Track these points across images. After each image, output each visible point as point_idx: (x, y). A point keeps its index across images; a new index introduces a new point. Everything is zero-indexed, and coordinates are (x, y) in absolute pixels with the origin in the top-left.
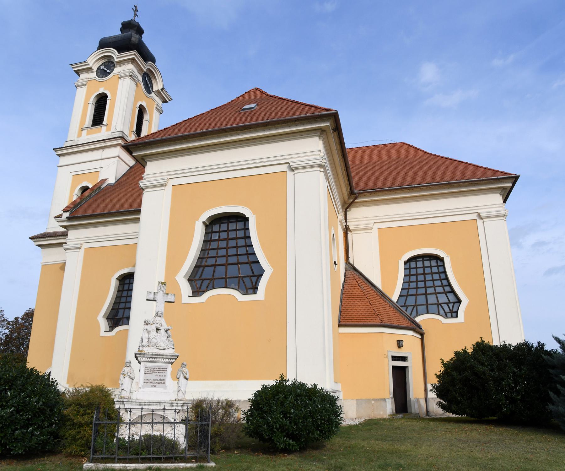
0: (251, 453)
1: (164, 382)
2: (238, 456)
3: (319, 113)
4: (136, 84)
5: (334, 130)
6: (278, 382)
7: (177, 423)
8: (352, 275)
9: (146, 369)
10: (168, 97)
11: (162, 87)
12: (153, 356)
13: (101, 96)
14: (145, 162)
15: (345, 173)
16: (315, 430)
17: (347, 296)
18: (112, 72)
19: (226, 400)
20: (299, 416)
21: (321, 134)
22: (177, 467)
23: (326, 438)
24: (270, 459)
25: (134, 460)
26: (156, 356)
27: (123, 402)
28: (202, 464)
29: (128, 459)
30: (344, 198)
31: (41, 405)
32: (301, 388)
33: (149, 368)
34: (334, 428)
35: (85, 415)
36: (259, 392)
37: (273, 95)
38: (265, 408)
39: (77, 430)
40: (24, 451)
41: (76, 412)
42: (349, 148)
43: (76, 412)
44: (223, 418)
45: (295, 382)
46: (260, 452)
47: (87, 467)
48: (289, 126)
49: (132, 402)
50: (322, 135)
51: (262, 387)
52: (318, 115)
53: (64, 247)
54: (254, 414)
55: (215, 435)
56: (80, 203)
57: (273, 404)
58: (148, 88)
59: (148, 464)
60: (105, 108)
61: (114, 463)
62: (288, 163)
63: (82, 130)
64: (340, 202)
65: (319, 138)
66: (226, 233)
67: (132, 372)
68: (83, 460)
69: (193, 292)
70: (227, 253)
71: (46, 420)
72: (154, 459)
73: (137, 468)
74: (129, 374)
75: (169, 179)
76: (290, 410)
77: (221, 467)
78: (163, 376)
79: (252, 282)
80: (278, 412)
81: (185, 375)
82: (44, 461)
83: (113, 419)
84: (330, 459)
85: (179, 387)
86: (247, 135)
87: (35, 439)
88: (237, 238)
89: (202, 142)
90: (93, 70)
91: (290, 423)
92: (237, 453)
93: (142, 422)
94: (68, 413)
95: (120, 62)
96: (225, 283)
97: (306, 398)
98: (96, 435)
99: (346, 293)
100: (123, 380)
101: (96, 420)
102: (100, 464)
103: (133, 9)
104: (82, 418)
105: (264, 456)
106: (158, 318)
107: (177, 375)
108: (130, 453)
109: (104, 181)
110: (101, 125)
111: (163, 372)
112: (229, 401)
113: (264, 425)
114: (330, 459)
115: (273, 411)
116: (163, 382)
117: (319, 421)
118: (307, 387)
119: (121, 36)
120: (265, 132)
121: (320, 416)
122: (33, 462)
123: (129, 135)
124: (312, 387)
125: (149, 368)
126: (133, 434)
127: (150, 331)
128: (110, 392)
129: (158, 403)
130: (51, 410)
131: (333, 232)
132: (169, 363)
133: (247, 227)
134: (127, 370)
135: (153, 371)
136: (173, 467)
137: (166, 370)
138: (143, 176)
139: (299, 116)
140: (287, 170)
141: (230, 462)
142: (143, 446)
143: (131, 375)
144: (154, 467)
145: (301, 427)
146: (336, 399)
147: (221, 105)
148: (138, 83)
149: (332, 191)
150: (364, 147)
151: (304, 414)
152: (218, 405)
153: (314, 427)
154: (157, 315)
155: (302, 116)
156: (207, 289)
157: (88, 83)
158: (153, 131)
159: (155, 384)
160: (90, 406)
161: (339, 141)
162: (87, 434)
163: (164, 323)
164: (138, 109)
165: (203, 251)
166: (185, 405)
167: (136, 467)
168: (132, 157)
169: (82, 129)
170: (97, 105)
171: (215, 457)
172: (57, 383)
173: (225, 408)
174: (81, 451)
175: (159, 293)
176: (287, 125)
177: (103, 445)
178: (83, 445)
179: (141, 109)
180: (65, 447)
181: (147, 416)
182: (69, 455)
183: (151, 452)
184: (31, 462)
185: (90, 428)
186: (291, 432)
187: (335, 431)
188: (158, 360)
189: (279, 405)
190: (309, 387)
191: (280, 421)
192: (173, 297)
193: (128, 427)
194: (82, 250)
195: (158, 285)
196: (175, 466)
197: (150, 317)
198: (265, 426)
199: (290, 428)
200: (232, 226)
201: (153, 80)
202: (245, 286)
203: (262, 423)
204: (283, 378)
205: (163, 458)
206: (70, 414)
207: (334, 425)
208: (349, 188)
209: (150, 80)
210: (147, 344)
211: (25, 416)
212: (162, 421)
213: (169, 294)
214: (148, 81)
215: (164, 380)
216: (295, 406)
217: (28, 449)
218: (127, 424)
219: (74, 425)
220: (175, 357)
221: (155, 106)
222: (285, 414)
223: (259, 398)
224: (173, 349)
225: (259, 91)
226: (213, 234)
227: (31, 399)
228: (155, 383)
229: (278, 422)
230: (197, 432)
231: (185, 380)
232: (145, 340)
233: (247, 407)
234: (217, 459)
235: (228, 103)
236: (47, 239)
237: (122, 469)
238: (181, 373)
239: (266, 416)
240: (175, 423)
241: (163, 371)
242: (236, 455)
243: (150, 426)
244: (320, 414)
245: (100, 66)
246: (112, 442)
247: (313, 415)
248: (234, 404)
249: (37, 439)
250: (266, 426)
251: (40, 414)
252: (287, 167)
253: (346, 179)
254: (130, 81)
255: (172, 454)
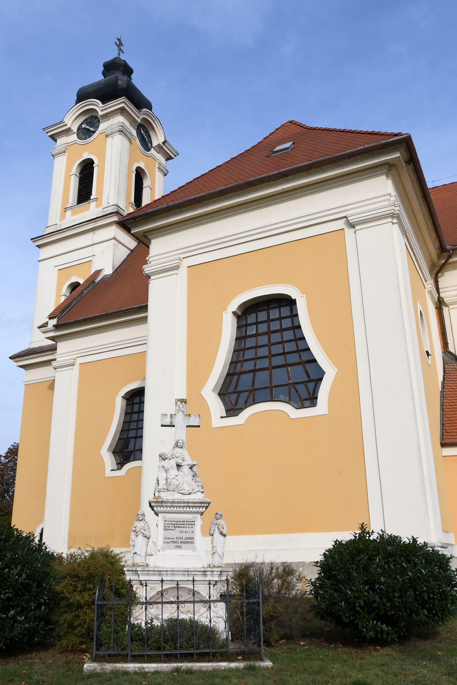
0: (325, 644)
1: (192, 540)
2: (306, 649)
3: (383, 141)
4: (130, 140)
5: (408, 162)
6: (357, 535)
7: (214, 601)
8: (454, 369)
9: (166, 523)
10: (173, 151)
11: (163, 140)
12: (175, 505)
13: (86, 163)
14: (148, 240)
15: (429, 222)
16: (420, 609)
17: (450, 401)
18: (97, 130)
19: (283, 564)
20: (394, 588)
21: (389, 170)
22: (216, 668)
23: (439, 622)
24: (354, 654)
25: (155, 657)
26: (179, 505)
27: (136, 571)
28: (252, 663)
29: (146, 656)
30: (431, 259)
31: (25, 579)
32: (392, 543)
33: (170, 521)
34: (449, 606)
35: (85, 591)
36: (329, 551)
37: (315, 126)
38: (341, 575)
39: (75, 613)
40: (4, 644)
41: (71, 588)
42: (432, 187)
43: (71, 588)
44: (279, 592)
45: (383, 535)
46: (338, 643)
47: (89, 668)
48: (342, 166)
49: (148, 571)
50: (391, 172)
51: (333, 543)
52: (382, 144)
53: (53, 364)
54: (324, 585)
55: (270, 618)
56: (69, 305)
57: (353, 570)
58: (146, 143)
59: (175, 663)
60: (93, 178)
61: (126, 662)
62: (346, 217)
63: (65, 211)
64: (427, 265)
65: (387, 177)
66: (266, 325)
67: (146, 528)
68: (85, 657)
69: (227, 411)
70: (270, 352)
71: (33, 600)
72: (183, 655)
73: (159, 669)
74: (143, 531)
75: (182, 259)
76: (379, 579)
77: (281, 669)
78: (191, 532)
79: (308, 390)
80: (361, 582)
81: (221, 529)
82: (31, 659)
83: (123, 597)
84: (449, 656)
85: (213, 548)
86: (284, 185)
87: (18, 628)
88: (281, 330)
89: (222, 203)
90: (73, 131)
91: (381, 598)
92: (304, 645)
93: (163, 601)
94: (62, 589)
95: (106, 115)
96: (270, 394)
97: (403, 559)
98: (100, 620)
99: (449, 396)
100: (135, 540)
101: (98, 600)
102: (107, 665)
103: (116, 43)
104: (81, 596)
105: (346, 649)
106: (178, 450)
107: (210, 530)
108: (149, 646)
109: (98, 272)
110: (89, 201)
111: (190, 526)
112: (288, 566)
113: (342, 602)
114: (449, 656)
115: (353, 580)
116: (190, 541)
117: (425, 594)
118: (402, 543)
119: (104, 81)
120: (307, 179)
121: (425, 586)
122: (16, 661)
123: (126, 209)
124: (410, 542)
125: (170, 521)
126: (152, 618)
127: (168, 469)
128: (118, 557)
129: (185, 571)
130: (39, 586)
131: (420, 308)
132: (197, 513)
133: (294, 313)
134: (139, 525)
135: (176, 526)
136: (211, 668)
137: (193, 523)
138: (147, 258)
139: (354, 150)
140: (344, 227)
141: (294, 660)
142: (167, 637)
143: (146, 533)
144: (184, 668)
145: (397, 604)
146: (449, 559)
147: (244, 151)
148: (132, 140)
149: (412, 250)
150: (454, 183)
151: (402, 584)
152: (271, 573)
153: (418, 605)
154: (177, 446)
155: (358, 148)
156: (247, 405)
157: (67, 149)
158: (157, 197)
159: (180, 544)
160: (90, 578)
161: (417, 177)
162: (89, 619)
163: (187, 457)
164: (135, 172)
165: (237, 352)
166: (224, 573)
167: (157, 668)
168: (131, 236)
169: (65, 210)
170: (81, 175)
171: (271, 651)
172: (46, 546)
173: (281, 577)
174: (82, 643)
175: (178, 414)
176: (339, 164)
177: (110, 635)
178: (84, 634)
179: (139, 173)
180: (60, 638)
181: (170, 591)
182: (64, 651)
183: (179, 645)
184: (14, 661)
185: (92, 610)
186: (382, 612)
187: (453, 610)
188: (181, 509)
189: (362, 571)
190: (405, 542)
191: (365, 595)
192: (198, 418)
193: (144, 607)
194: (77, 366)
195: (176, 404)
196: (213, 667)
197: (168, 449)
198: (343, 603)
199: (381, 606)
200: (274, 314)
201: (151, 132)
202: (299, 396)
203: (338, 599)
204: (365, 530)
205: (195, 654)
206: (65, 591)
207: (450, 601)
208: (437, 244)
209: (147, 132)
210: (165, 487)
211: (4, 595)
212: (192, 599)
213: (191, 415)
214: (144, 134)
215: (192, 538)
216: (387, 572)
217: (9, 642)
218: (142, 603)
219: (69, 606)
220: (205, 505)
221: (157, 166)
222: (371, 584)
223: (330, 561)
224: (202, 492)
225: (294, 124)
226: (248, 328)
227: (10, 571)
228: (180, 542)
229: (361, 597)
230: (242, 613)
231: (222, 537)
232: (162, 482)
233: (313, 574)
234: (274, 655)
235: (253, 147)
236: (31, 357)
237: (139, 671)
238: (215, 527)
239: (343, 588)
240: (210, 602)
241: (190, 525)
242: (302, 649)
243: (175, 606)
244: (425, 583)
245: (81, 125)
246: (124, 629)
247: (415, 586)
248: (295, 571)
249: (21, 627)
250: (344, 603)
251: (24, 591)
252: (345, 223)
253: (432, 230)
254: (122, 138)
255: (208, 647)
